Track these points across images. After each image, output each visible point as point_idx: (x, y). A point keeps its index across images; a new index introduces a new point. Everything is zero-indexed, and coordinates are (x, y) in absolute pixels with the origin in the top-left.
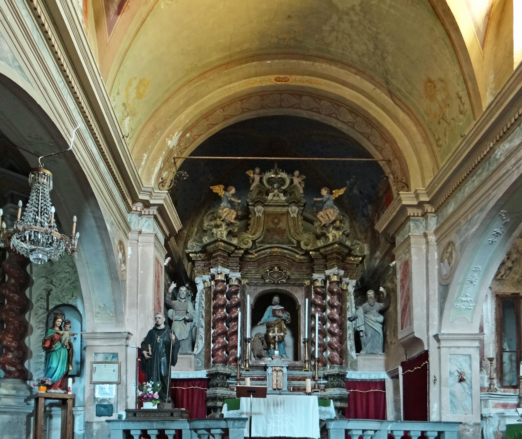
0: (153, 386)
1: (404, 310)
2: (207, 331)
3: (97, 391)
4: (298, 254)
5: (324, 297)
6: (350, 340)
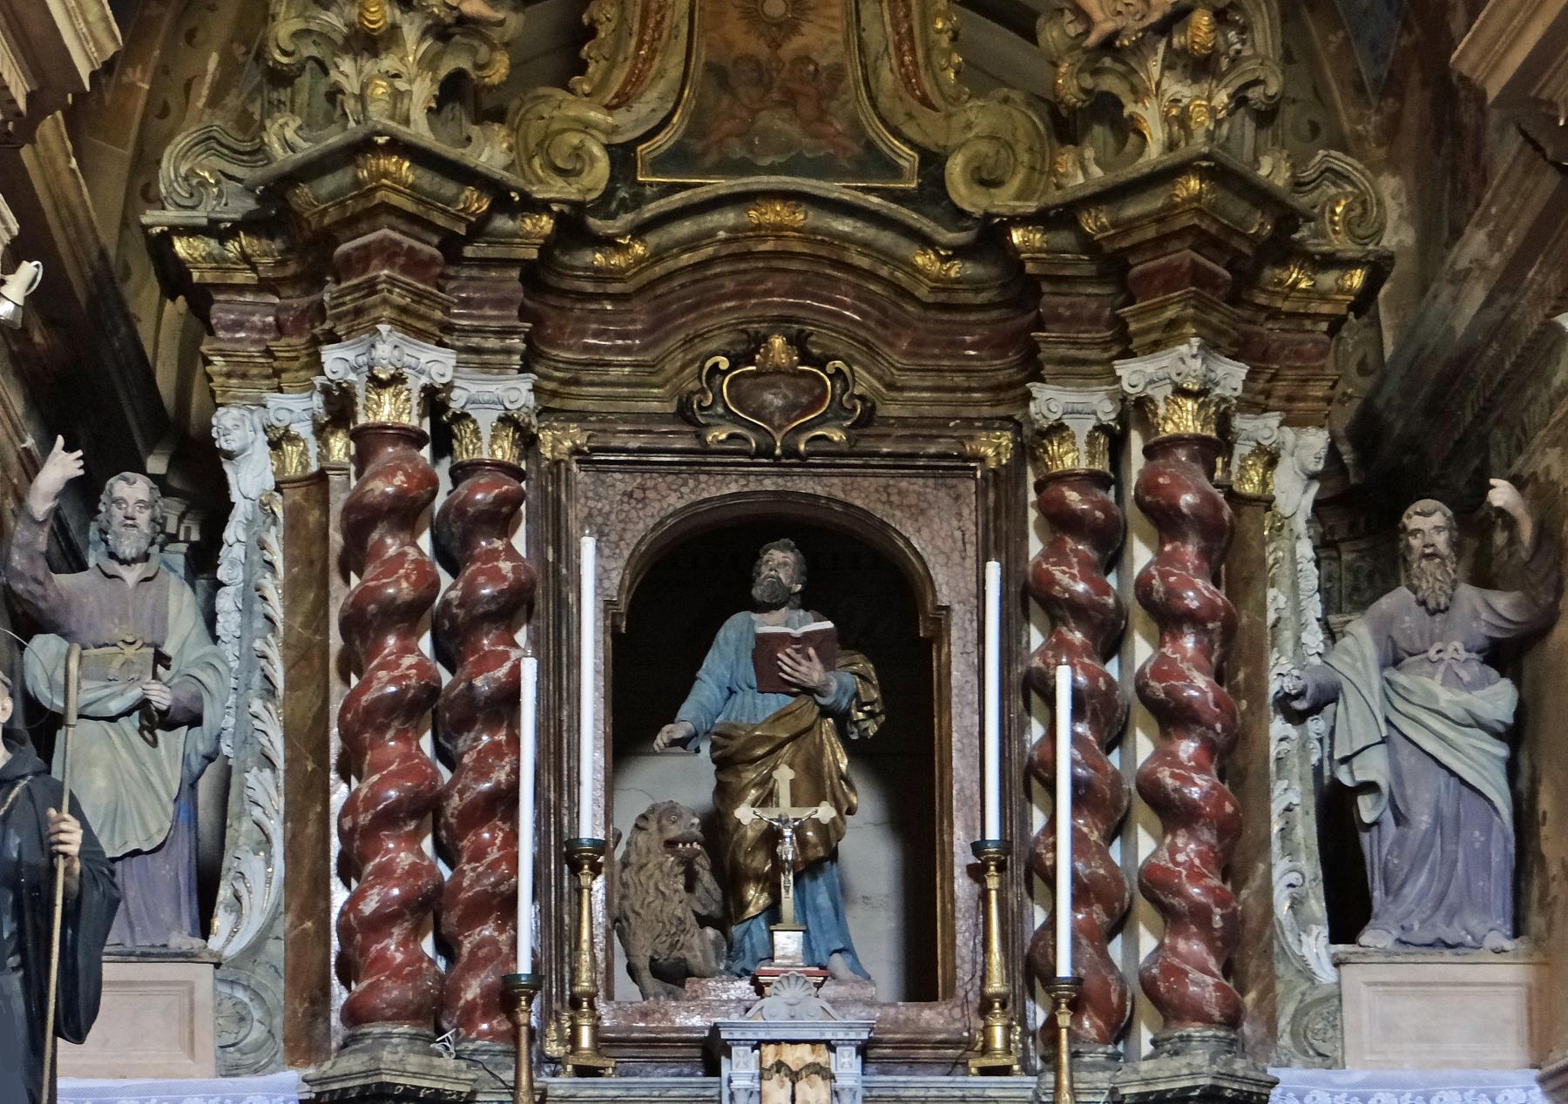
2: (305, 793)
5: (1109, 547)
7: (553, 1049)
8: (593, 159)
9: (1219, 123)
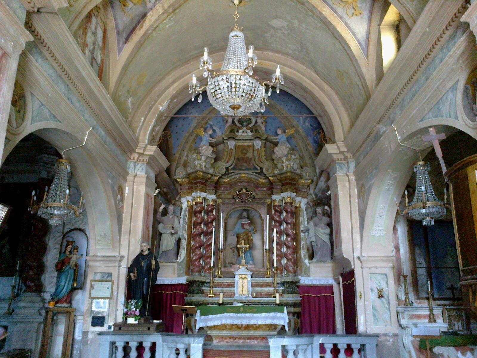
0: (136, 303)
2: (189, 243)
3: (94, 304)
4: (261, 178)
5: (281, 213)
6: (303, 249)
7: (216, 274)
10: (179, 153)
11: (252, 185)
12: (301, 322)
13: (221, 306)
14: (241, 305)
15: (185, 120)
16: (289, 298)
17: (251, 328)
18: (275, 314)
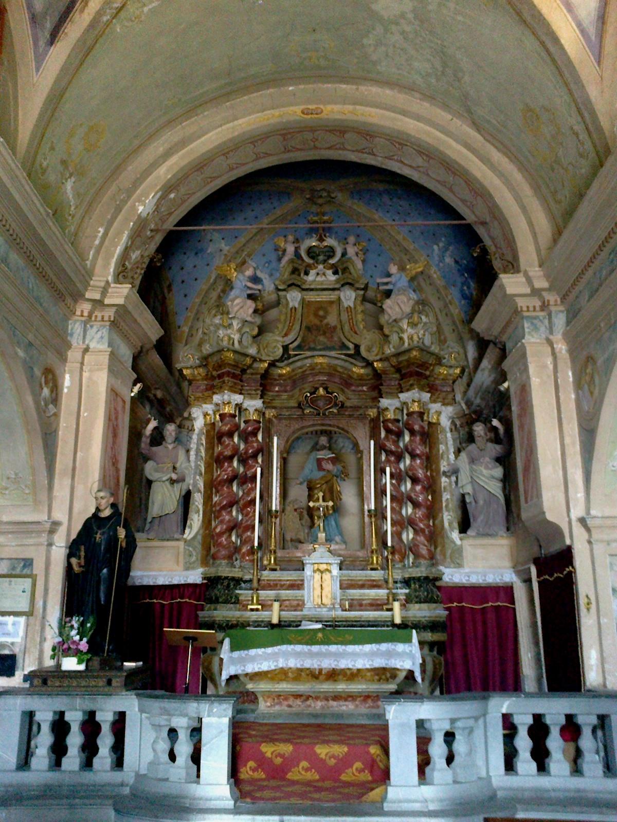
1: (526, 470)
2: (208, 499)
4: (355, 365)
5: (399, 434)
6: (448, 510)
7: (265, 562)
8: (279, 349)
9: (420, 339)
10: (190, 324)
11: (337, 380)
12: (446, 661)
13: (276, 631)
14: (319, 626)
15: (200, 255)
16: (422, 612)
17: (340, 677)
18: (393, 647)
